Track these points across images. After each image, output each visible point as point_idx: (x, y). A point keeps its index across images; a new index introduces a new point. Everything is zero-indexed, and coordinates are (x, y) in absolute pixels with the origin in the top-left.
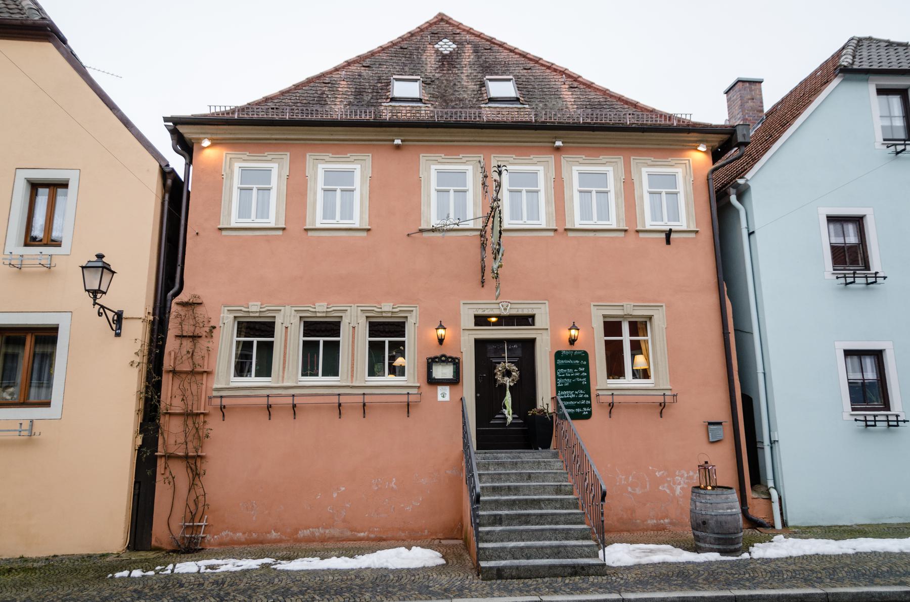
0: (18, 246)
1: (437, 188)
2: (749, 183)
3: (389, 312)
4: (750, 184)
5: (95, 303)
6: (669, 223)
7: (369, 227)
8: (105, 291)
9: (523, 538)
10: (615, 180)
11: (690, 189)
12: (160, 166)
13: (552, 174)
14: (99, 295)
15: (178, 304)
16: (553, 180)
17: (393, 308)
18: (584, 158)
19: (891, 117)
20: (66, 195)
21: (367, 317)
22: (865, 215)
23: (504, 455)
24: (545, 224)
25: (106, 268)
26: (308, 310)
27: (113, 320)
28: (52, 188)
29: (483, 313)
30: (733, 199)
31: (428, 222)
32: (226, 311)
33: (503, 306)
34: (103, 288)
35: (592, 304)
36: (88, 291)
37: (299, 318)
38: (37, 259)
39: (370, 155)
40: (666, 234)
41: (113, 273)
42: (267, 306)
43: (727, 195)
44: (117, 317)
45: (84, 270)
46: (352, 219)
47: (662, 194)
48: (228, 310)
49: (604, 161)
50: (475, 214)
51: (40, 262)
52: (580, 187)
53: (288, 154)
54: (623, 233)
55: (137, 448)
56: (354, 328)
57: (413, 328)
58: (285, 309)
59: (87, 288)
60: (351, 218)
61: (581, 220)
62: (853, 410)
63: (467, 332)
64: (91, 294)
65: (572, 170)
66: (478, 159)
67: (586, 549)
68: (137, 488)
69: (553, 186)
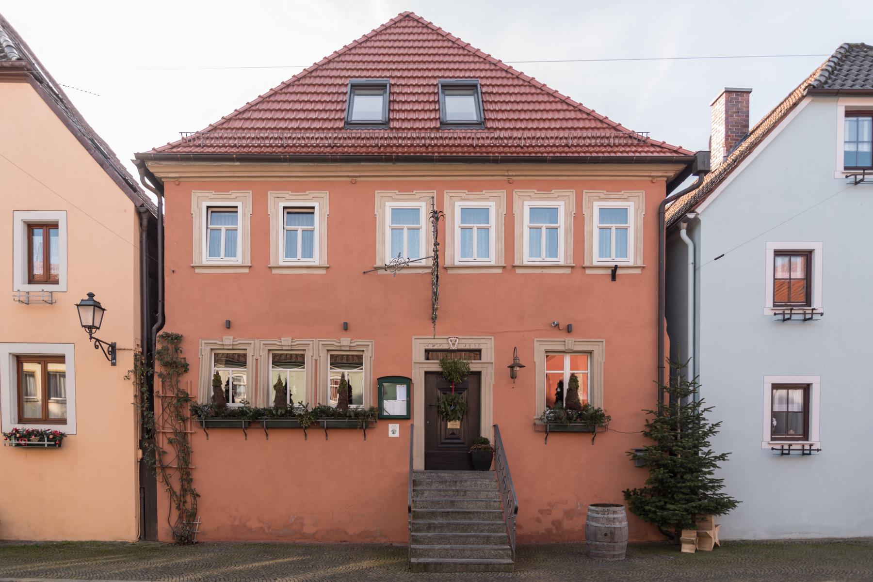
0: (24, 284)
1: (461, 225)
2: (699, 216)
3: (347, 346)
4: (700, 218)
5: (91, 338)
6: (547, 259)
7: (328, 266)
8: (98, 326)
9: (451, 541)
10: (566, 214)
11: (641, 222)
12: (136, 206)
13: (503, 210)
14: (94, 330)
15: (162, 337)
16: (504, 216)
17: (351, 343)
18: (536, 192)
19: (857, 142)
20: (57, 235)
21: (328, 351)
22: (814, 250)
23: (446, 475)
24: (563, 260)
25: (97, 306)
26: (275, 344)
27: (109, 352)
28: (45, 228)
29: (433, 348)
30: (683, 233)
31: (383, 260)
32: (203, 344)
33: (451, 341)
34: (97, 324)
35: (536, 339)
36: (85, 327)
37: (267, 352)
38: (40, 296)
39: (328, 192)
40: (612, 270)
41: (104, 310)
42: (356, 341)
43: (678, 229)
44: (112, 348)
45: (79, 308)
46: (312, 257)
47: (612, 230)
48: (205, 343)
49: (556, 195)
50: (427, 252)
51: (42, 299)
52: (600, 223)
53: (251, 192)
54: (570, 269)
55: (139, 460)
56: (257, 360)
57: (369, 360)
58: (313, 343)
59: (83, 324)
60: (311, 256)
61: (530, 257)
62: (772, 439)
63: (418, 365)
64: (87, 329)
65: (523, 205)
66: (431, 195)
67: (501, 552)
68: (142, 492)
69: (503, 223)
